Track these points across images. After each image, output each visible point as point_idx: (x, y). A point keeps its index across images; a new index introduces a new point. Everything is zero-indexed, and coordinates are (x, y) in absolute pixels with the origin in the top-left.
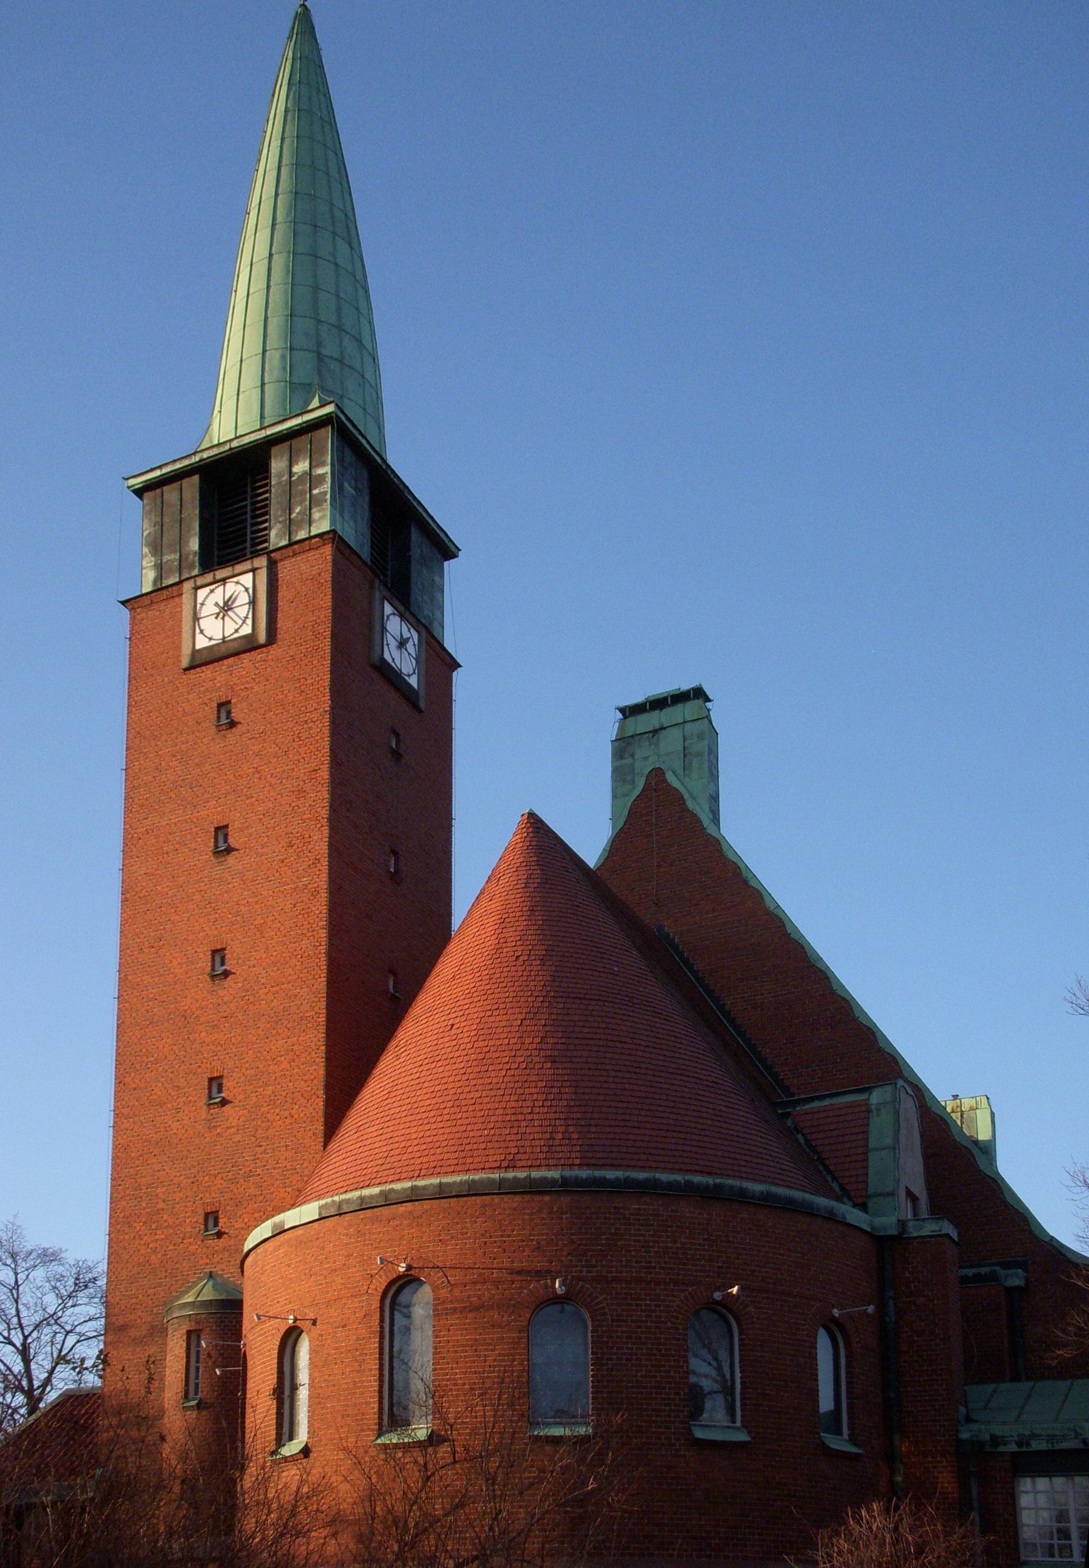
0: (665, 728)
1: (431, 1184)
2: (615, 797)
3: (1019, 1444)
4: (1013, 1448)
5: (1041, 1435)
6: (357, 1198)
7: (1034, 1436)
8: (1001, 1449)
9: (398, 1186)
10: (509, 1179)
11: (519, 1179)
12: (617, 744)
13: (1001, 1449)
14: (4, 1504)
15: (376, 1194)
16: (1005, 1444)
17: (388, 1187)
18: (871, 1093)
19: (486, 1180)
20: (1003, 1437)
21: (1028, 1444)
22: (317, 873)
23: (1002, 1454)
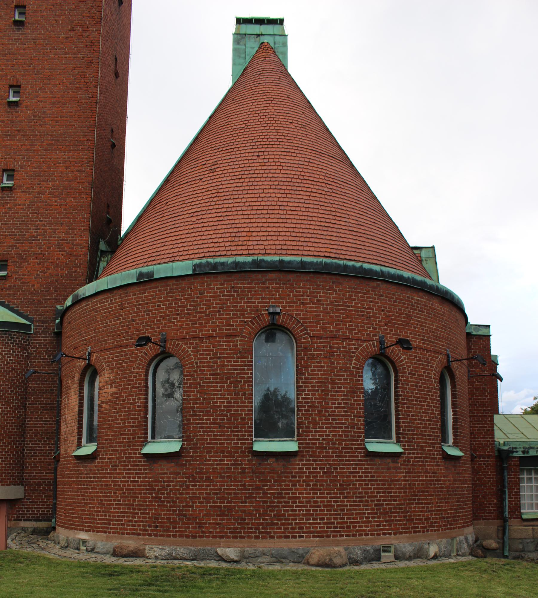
0: (264, 35)
1: (294, 261)
2: (234, 64)
3: (524, 452)
4: (520, 454)
5: (534, 448)
6: (232, 263)
7: (531, 448)
8: (515, 454)
9: (268, 258)
10: (350, 266)
11: (356, 267)
12: (236, 36)
13: (515, 454)
14: (298, 596)
15: (249, 262)
16: (517, 452)
17: (260, 257)
18: (421, 251)
19: (335, 264)
20: (516, 448)
21: (528, 452)
22: (92, 51)
23: (515, 457)
